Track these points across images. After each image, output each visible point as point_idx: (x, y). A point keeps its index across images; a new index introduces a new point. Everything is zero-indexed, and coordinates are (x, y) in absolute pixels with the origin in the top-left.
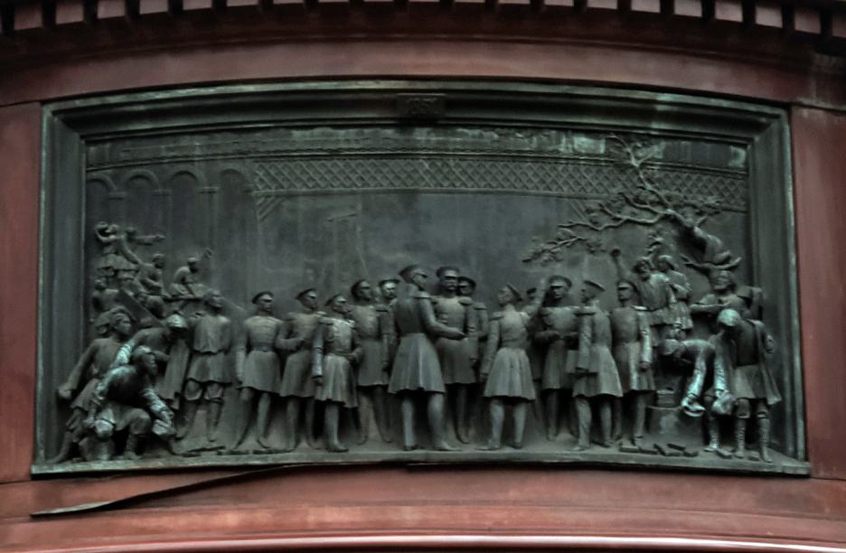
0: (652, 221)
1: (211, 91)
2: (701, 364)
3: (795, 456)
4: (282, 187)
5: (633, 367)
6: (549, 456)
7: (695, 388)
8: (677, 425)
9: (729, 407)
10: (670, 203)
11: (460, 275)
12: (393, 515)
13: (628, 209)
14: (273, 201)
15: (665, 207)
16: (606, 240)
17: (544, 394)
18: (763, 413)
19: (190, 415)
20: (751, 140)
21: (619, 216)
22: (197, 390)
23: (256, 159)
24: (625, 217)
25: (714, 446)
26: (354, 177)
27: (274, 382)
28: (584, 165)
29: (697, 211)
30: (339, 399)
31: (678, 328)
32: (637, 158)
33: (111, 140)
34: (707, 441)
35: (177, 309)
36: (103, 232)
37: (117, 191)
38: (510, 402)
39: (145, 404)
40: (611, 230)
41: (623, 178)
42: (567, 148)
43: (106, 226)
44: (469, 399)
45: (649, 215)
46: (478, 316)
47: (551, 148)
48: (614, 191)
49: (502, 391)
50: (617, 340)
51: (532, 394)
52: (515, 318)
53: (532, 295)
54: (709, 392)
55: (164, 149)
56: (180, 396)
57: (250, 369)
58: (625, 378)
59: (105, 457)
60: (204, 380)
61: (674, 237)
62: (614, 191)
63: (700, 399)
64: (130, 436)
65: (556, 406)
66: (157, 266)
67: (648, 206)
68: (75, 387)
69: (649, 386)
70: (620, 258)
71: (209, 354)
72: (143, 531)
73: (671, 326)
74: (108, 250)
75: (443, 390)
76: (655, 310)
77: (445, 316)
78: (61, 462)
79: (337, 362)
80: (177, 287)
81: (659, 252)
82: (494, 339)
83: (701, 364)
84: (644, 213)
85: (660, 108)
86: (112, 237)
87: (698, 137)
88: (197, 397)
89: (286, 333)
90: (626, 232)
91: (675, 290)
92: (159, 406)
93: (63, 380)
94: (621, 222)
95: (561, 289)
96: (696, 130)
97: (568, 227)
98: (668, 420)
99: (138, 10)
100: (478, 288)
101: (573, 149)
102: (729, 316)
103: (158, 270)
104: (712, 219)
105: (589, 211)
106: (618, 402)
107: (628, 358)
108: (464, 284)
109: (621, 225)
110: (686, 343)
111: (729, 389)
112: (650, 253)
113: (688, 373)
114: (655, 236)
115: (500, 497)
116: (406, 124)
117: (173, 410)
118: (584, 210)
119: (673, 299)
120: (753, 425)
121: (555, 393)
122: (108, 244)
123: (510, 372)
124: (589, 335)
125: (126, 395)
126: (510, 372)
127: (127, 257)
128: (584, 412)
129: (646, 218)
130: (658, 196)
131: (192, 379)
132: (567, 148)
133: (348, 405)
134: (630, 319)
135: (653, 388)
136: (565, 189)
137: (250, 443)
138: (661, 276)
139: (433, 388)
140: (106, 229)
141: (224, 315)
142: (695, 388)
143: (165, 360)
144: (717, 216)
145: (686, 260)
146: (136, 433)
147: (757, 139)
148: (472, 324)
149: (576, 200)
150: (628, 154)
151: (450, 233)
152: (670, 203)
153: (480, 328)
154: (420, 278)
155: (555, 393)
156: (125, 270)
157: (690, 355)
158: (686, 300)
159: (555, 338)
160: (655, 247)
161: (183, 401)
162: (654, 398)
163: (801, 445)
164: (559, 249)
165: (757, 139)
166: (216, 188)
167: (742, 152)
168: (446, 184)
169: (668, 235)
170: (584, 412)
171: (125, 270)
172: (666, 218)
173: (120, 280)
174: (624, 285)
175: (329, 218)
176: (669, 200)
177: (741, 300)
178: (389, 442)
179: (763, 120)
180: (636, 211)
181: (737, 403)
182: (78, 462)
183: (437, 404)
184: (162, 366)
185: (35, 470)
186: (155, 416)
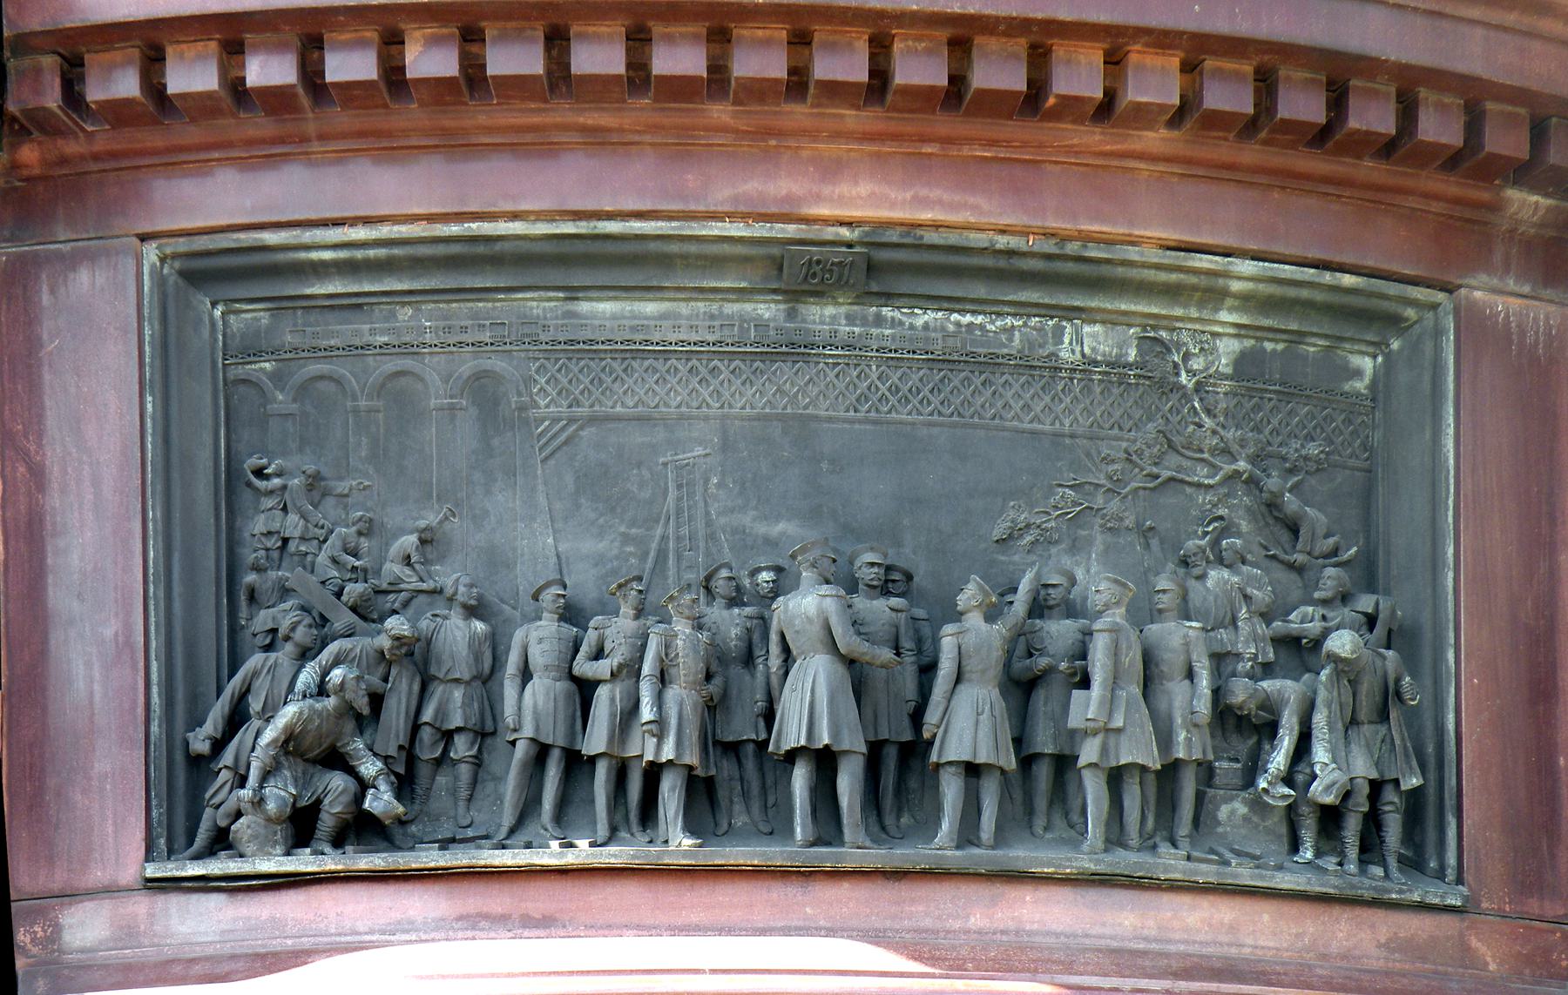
0: (1211, 482)
1: (454, 229)
3: (1440, 875)
7: (1279, 760)
11: (889, 562)
14: (563, 429)
17: (1027, 761)
18: (1392, 803)
21: (1155, 470)
22: (435, 743)
24: (1166, 474)
26: (705, 393)
27: (572, 735)
31: (1249, 659)
32: (1192, 373)
33: (1103, 322)
36: (259, 473)
38: (972, 770)
42: (1073, 351)
43: (264, 461)
46: (917, 631)
49: (951, 755)
51: (1010, 762)
53: (1009, 598)
54: (1301, 767)
56: (409, 752)
58: (1165, 739)
61: (1248, 509)
63: (1288, 780)
67: (1206, 456)
68: (219, 736)
69: (1204, 752)
73: (1238, 656)
75: (864, 749)
78: (197, 857)
82: (946, 667)
85: (1236, 286)
86: (276, 481)
90: (1169, 499)
91: (1247, 598)
92: (370, 768)
93: (196, 722)
95: (1060, 589)
97: (1070, 487)
99: (321, 74)
101: (1083, 355)
102: (1342, 643)
103: (362, 539)
104: (1313, 481)
105: (1108, 460)
106: (1152, 777)
107: (1170, 706)
109: (1161, 484)
110: (1265, 684)
114: (1215, 506)
117: (397, 775)
119: (1243, 613)
120: (1373, 821)
121: (1047, 760)
128: (1094, 790)
129: (1201, 474)
133: (699, 772)
134: (1176, 641)
135: (1211, 757)
136: (1067, 422)
138: (1226, 573)
139: (845, 746)
142: (1279, 760)
143: (380, 691)
147: (1395, 345)
148: (907, 643)
150: (1176, 365)
153: (919, 651)
155: (1047, 760)
159: (1049, 671)
162: (1207, 772)
163: (1451, 860)
167: (1367, 364)
170: (1094, 790)
173: (813, 515)
178: (173, 961)
179: (1410, 313)
180: (1186, 463)
182: (231, 857)
185: (152, 871)
186: (363, 785)
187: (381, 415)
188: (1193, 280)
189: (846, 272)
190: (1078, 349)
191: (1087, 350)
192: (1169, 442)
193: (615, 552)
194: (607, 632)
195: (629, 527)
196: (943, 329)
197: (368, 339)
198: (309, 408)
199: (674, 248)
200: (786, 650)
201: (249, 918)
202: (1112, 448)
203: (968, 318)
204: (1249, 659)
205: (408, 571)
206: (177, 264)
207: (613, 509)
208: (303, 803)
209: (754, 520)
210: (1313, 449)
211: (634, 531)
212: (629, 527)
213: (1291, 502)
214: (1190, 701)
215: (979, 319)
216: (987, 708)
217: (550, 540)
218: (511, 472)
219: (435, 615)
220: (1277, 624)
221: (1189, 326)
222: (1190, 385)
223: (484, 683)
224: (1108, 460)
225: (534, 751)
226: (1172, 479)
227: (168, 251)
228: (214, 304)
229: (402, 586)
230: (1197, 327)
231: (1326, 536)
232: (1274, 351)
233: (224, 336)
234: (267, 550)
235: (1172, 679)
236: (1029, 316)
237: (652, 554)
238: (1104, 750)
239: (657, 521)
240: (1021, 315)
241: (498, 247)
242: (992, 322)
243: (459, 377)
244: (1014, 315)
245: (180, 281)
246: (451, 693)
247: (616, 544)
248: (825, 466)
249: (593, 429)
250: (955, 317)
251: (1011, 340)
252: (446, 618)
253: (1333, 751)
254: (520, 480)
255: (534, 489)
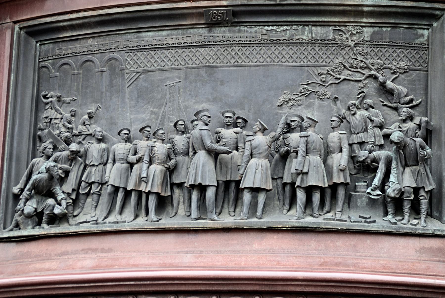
2: (382, 168)
4: (140, 67)
5: (335, 168)
6: (280, 223)
7: (376, 182)
8: (367, 204)
9: (396, 192)
10: (373, 68)
12: (177, 260)
13: (346, 72)
15: (371, 69)
16: (330, 92)
19: (82, 202)
20: (431, 25)
21: (338, 76)
22: (87, 187)
23: (128, 51)
24: (343, 77)
25: (390, 217)
28: (318, 46)
29: (392, 71)
30: (155, 190)
31: (372, 144)
34: (386, 214)
35: (81, 140)
36: (45, 97)
37: (54, 73)
38: (255, 191)
39: (52, 195)
40: (334, 85)
41: (343, 52)
42: (308, 37)
43: (47, 93)
44: (230, 190)
45: (359, 75)
47: (297, 37)
48: (337, 61)
50: (326, 153)
52: (261, 140)
55: (77, 47)
56: (76, 190)
57: (113, 175)
58: (329, 174)
59: (30, 227)
60: (90, 181)
62: (337, 61)
64: (44, 215)
65: (288, 193)
66: (72, 116)
70: (338, 103)
71: (93, 165)
72: (41, 270)
74: (47, 107)
76: (358, 133)
77: (224, 140)
79: (157, 169)
80: (81, 127)
81: (364, 97)
83: (382, 168)
84: (356, 74)
87: (395, 26)
88: (86, 191)
89: (133, 152)
90: (345, 86)
91: (372, 121)
92: (60, 196)
94: (340, 80)
95: (296, 122)
96: (393, 21)
98: (362, 201)
100: (248, 123)
101: (312, 37)
103: (73, 118)
104: (403, 76)
105: (320, 74)
107: (333, 163)
108: (240, 120)
109: (341, 82)
111: (402, 180)
112: (358, 98)
113: (375, 170)
115: (248, 248)
116: (213, 24)
118: (317, 73)
119: (370, 126)
122: (47, 104)
123: (256, 173)
124: (304, 149)
125: (44, 190)
126: (256, 173)
127: (57, 111)
128: (301, 196)
129: (357, 77)
130: (365, 63)
131: (83, 181)
132: (308, 37)
137: (112, 218)
140: (47, 95)
141: (103, 142)
144: (406, 74)
145: (383, 102)
146: (47, 213)
147: (435, 25)
149: (312, 68)
151: (233, 91)
152: (373, 68)
154: (205, 118)
156: (55, 119)
157: (376, 160)
158: (381, 127)
160: (361, 95)
161: (78, 194)
164: (300, 98)
165: (435, 25)
166: (105, 69)
167: (426, 32)
168: (233, 61)
169: (372, 86)
170: (301, 196)
171: (55, 119)
172: (370, 76)
174: (334, 118)
175: (165, 84)
176: (373, 66)
177: (416, 125)
179: (438, 12)
180: (351, 73)
181: (403, 190)
183: (210, 193)
184: (67, 173)
187: (81, 75)
188: (349, 8)
189: (225, 16)
190: (310, 35)
191: (314, 35)
192: (344, 66)
193: (148, 117)
194: (137, 146)
195: (153, 108)
196: (262, 32)
197: (79, 50)
198: (61, 74)
199: (185, 11)
200: (194, 149)
201: (21, 252)
202: (321, 69)
203: (271, 28)
204: (372, 144)
205: (84, 127)
206: (25, 30)
207: (149, 102)
208: (39, 210)
209: (194, 103)
210: (402, 64)
211: (154, 110)
212: (153, 108)
213: (390, 84)
214: (340, 160)
215: (275, 28)
216: (260, 167)
217: (128, 114)
218: (117, 92)
219: (89, 143)
220: (385, 130)
221: (352, 24)
222: (352, 45)
223: (104, 165)
224: (320, 74)
225: (113, 189)
226: (345, 79)
227: (21, 26)
228: (37, 42)
229: (83, 133)
230: (355, 24)
231: (406, 96)
232: (387, 30)
233: (40, 52)
234: (46, 123)
235: (334, 153)
236: (292, 25)
237: (160, 117)
238: (302, 180)
239: (163, 105)
240: (290, 25)
241: (114, 16)
242: (279, 28)
243: (104, 60)
244: (287, 25)
245: (26, 35)
246: (92, 169)
247: (149, 115)
248: (219, 83)
249: (144, 75)
250: (266, 28)
251: (286, 34)
252: (92, 143)
253: (398, 177)
254: (120, 94)
255: (124, 97)
